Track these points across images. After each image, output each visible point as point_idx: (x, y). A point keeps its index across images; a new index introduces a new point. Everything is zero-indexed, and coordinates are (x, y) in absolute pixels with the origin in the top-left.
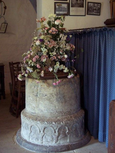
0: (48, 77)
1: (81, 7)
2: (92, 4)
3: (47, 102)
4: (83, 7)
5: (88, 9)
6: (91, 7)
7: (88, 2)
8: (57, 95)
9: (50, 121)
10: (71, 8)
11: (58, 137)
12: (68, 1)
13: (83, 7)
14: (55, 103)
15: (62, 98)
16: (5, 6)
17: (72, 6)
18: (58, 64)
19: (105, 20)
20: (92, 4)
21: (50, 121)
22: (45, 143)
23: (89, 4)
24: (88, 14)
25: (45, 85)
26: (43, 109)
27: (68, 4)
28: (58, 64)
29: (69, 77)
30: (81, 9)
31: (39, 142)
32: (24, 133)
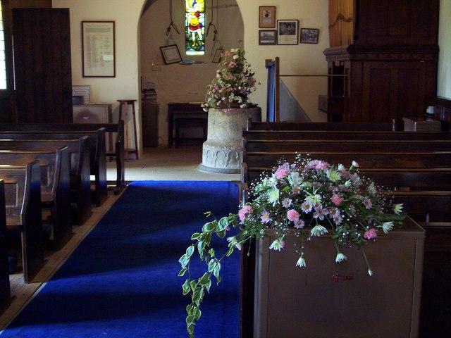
0: (222, 107)
1: (292, 34)
2: (306, 31)
3: (221, 129)
4: (295, 34)
5: (301, 37)
6: (305, 35)
7: (302, 29)
8: (230, 123)
9: (222, 146)
10: (279, 36)
11: (228, 161)
12: (276, 29)
13: (295, 34)
14: (228, 130)
15: (234, 126)
16: (214, 44)
17: (280, 34)
18: (232, 95)
19: (324, 49)
20: (306, 31)
21: (222, 146)
22: (218, 167)
23: (303, 30)
24: (262, 42)
25: (220, 114)
26: (218, 135)
27: (276, 32)
28: (232, 95)
29: (242, 106)
30: (292, 36)
31: (212, 166)
32: (204, 163)
